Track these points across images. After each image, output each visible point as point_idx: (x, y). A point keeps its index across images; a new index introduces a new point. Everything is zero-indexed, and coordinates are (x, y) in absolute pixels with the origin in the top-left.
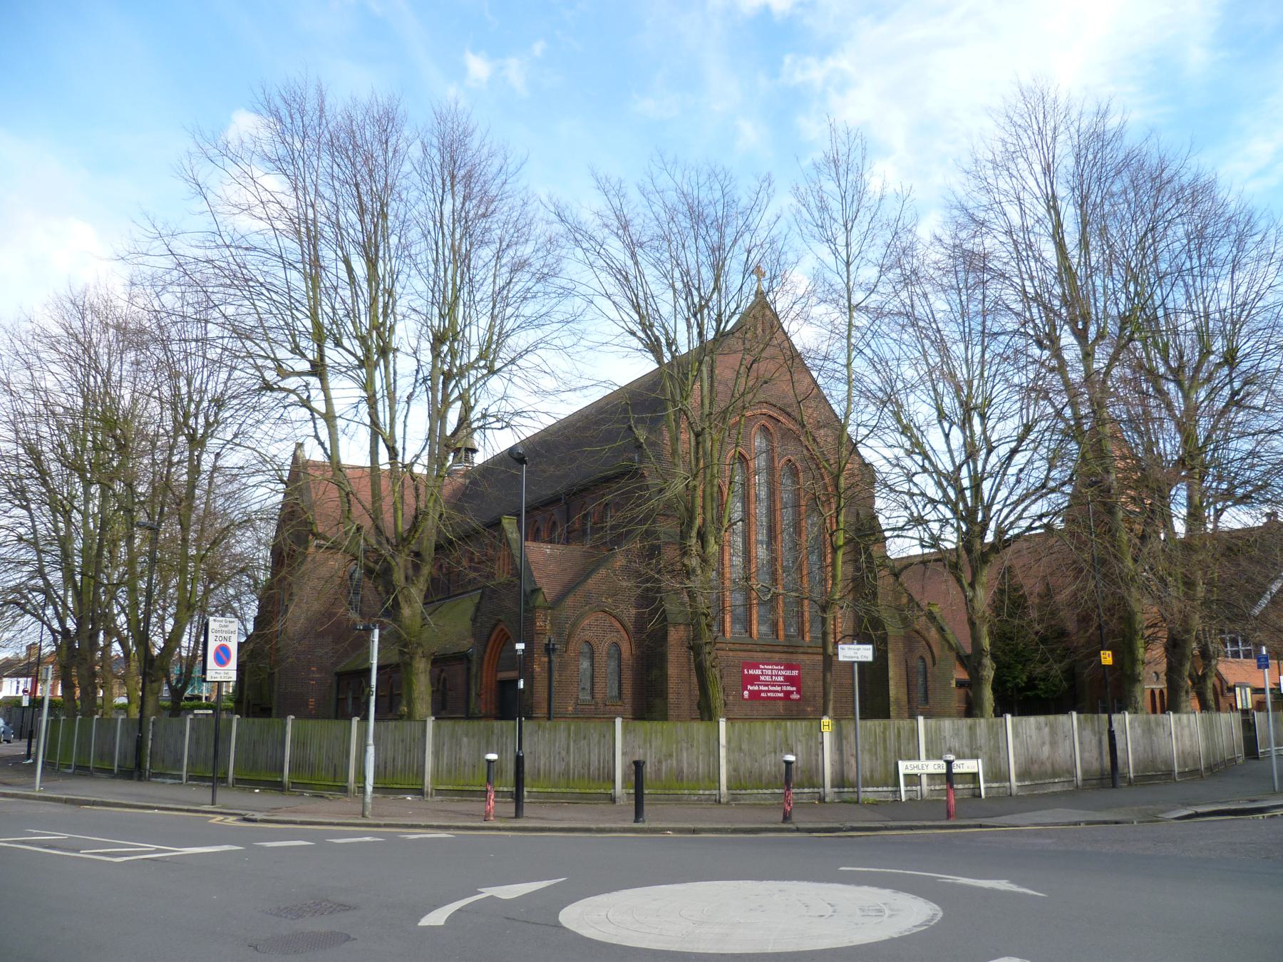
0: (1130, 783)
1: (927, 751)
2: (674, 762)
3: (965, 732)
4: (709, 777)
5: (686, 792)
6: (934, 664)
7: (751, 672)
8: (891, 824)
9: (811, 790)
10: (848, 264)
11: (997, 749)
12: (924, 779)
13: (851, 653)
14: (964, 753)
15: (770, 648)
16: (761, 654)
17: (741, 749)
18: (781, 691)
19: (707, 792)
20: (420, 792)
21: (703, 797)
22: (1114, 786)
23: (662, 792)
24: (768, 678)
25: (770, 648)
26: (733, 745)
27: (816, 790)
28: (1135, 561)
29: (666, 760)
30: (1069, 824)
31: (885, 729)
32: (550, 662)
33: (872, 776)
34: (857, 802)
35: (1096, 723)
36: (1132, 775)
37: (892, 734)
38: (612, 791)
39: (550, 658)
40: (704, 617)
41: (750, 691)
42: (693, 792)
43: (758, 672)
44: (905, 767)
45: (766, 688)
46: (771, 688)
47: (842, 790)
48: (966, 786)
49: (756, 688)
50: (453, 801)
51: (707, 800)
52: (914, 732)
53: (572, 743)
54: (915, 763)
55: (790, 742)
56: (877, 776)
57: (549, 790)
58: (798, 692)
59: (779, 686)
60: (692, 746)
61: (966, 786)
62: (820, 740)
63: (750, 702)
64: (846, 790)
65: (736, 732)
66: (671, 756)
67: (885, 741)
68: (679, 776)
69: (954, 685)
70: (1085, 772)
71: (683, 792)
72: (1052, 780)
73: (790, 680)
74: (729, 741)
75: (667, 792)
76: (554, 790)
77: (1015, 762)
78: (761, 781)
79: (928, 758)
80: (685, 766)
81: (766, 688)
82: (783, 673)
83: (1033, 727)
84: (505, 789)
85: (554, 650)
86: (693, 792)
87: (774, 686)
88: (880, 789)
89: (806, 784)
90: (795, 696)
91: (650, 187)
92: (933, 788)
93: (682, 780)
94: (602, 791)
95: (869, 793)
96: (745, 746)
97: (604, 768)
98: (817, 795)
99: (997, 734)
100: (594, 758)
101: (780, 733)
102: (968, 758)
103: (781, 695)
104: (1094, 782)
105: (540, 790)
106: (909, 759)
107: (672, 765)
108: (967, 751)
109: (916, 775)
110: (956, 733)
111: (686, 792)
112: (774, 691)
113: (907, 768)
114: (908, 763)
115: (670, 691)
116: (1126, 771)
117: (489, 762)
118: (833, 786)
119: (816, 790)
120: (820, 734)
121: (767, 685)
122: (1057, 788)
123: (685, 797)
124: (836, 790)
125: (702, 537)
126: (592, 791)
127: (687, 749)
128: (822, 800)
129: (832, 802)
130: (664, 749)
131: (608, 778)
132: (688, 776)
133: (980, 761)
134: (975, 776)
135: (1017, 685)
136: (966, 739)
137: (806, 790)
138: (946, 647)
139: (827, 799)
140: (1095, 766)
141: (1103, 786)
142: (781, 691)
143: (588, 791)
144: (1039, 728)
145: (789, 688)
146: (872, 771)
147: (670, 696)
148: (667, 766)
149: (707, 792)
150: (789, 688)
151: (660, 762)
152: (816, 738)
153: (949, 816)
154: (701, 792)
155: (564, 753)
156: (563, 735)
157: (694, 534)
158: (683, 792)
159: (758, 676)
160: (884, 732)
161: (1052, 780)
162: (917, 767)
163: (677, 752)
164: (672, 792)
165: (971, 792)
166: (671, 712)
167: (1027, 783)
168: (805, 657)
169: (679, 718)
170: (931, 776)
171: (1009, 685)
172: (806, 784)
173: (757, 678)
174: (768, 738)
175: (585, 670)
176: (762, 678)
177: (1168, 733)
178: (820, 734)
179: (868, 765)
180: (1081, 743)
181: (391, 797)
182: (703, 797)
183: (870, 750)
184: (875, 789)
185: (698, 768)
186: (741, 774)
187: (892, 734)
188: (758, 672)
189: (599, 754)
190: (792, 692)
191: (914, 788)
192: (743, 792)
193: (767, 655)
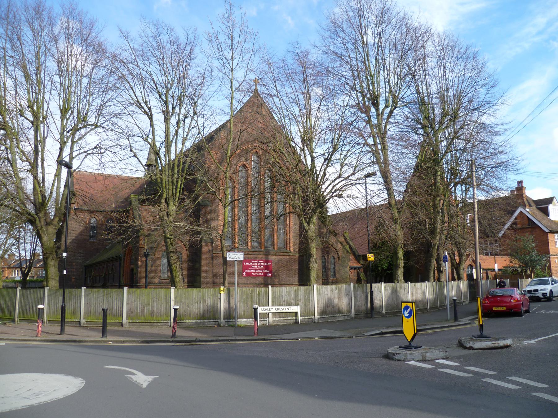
0: (383, 316)
1: (273, 302)
2: (150, 308)
3: (293, 293)
4: (166, 314)
5: (155, 321)
6: (339, 259)
7: (247, 264)
8: (238, 338)
9: (214, 320)
10: (232, 70)
11: (309, 301)
12: (270, 315)
13: (233, 256)
14: (291, 303)
15: (257, 253)
16: (252, 256)
17: (181, 302)
18: (262, 272)
19: (165, 322)
20: (13, 320)
21: (163, 324)
22: (371, 317)
23: (145, 321)
24: (255, 267)
25: (257, 253)
26: (178, 299)
27: (216, 320)
28: (399, 212)
29: (147, 307)
30: (308, 338)
31: (252, 291)
32: (146, 260)
33: (244, 314)
34: (235, 326)
35: (365, 288)
36: (384, 312)
37: (255, 295)
38: (122, 321)
39: (146, 259)
40: (169, 240)
41: (246, 272)
42: (158, 321)
43: (251, 264)
44: (260, 310)
45: (255, 271)
46: (257, 271)
47: (229, 320)
48: (292, 318)
49: (250, 271)
50: (55, 326)
51: (165, 325)
52: (267, 293)
53: (105, 299)
54: (266, 308)
55: (204, 298)
56: (247, 314)
57: (95, 321)
58: (271, 272)
59: (261, 270)
60: (158, 300)
61: (292, 318)
62: (219, 297)
63: (246, 278)
64: (231, 320)
65: (179, 294)
66: (149, 305)
67: (252, 298)
68: (152, 314)
69: (349, 269)
70: (356, 311)
71: (154, 321)
72: (338, 315)
73: (267, 267)
74: (176, 298)
75: (147, 321)
76: (97, 321)
77: (318, 307)
78: (190, 316)
79: (273, 305)
80: (155, 309)
81: (255, 271)
82: (263, 264)
83: (329, 290)
84: (77, 320)
85: (148, 254)
86: (158, 321)
87: (259, 270)
88: (248, 320)
89: (212, 318)
90: (270, 275)
91: (143, 35)
92: (275, 319)
93: (153, 316)
94: (118, 321)
95: (242, 322)
96: (183, 300)
97: (119, 310)
98: (217, 323)
99: (309, 294)
100: (115, 306)
101: (200, 294)
102: (294, 305)
103: (262, 274)
104: (362, 315)
105: (91, 321)
106: (264, 306)
107: (149, 309)
108: (293, 302)
109: (267, 313)
110: (288, 293)
111: (155, 321)
112: (258, 273)
113: (262, 310)
114: (263, 308)
115: (202, 273)
116: (381, 310)
117: (39, 309)
118: (224, 319)
119: (216, 320)
120: (219, 294)
121: (255, 270)
122: (340, 319)
123: (155, 324)
124: (226, 320)
125: (167, 203)
126: (113, 321)
127: (156, 301)
128: (219, 325)
129: (224, 326)
130: (146, 301)
131: (120, 315)
132: (156, 314)
133: (299, 306)
134: (297, 313)
135: (383, 268)
136: (293, 297)
137: (212, 321)
138: (345, 252)
139: (222, 325)
140: (363, 308)
141: (367, 317)
142: (262, 272)
143: (111, 321)
144: (332, 291)
145: (266, 271)
146: (244, 312)
147: (203, 275)
148: (147, 310)
149: (165, 322)
150: (266, 271)
151: (144, 307)
152: (217, 296)
153: (254, 334)
154: (162, 321)
155: (101, 304)
156: (102, 295)
157: (163, 201)
158: (154, 321)
159: (251, 265)
160: (251, 293)
161: (338, 315)
162: (267, 310)
163: (152, 303)
164: (149, 321)
165: (294, 321)
166: (202, 283)
167: (324, 316)
168: (274, 257)
169: (207, 285)
170: (274, 314)
171: (379, 268)
172: (212, 318)
173: (250, 266)
174: (194, 296)
175: (165, 264)
176: (253, 267)
177: (406, 292)
178: (219, 294)
179: (242, 309)
180: (355, 297)
181: (31, 324)
182: (163, 324)
183: (244, 302)
184: (246, 320)
185: (161, 310)
186: (181, 313)
187: (255, 295)
188: (251, 264)
189: (117, 304)
190: (268, 273)
191: (265, 319)
192: (182, 321)
193: (255, 256)
